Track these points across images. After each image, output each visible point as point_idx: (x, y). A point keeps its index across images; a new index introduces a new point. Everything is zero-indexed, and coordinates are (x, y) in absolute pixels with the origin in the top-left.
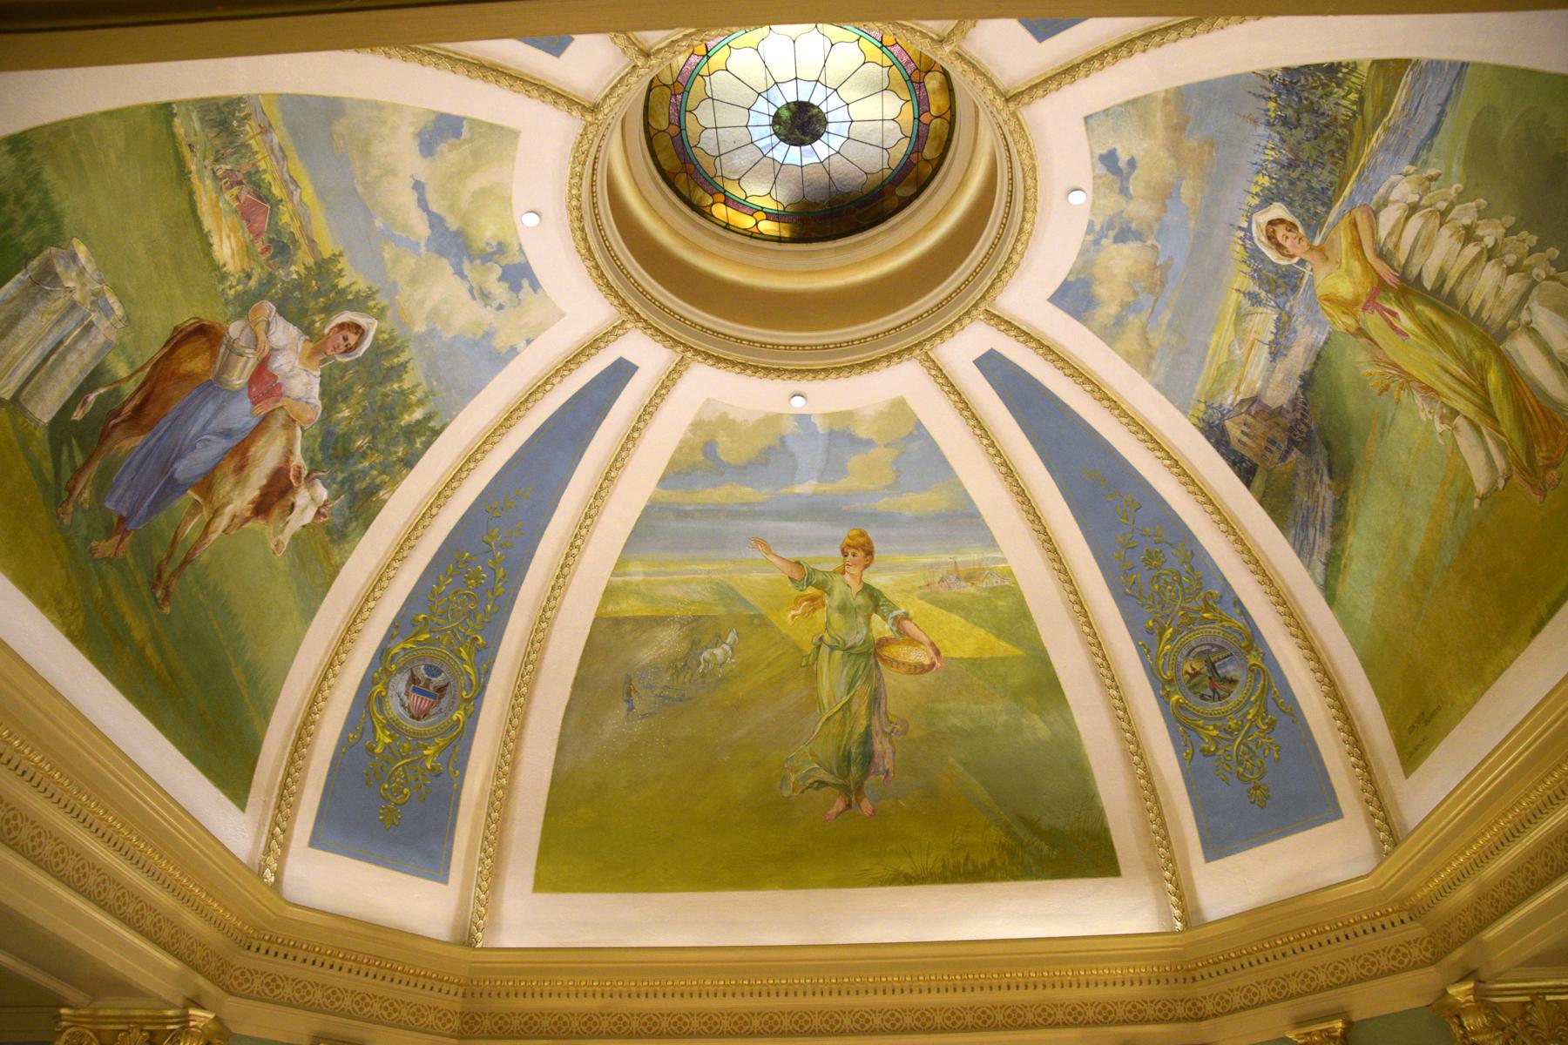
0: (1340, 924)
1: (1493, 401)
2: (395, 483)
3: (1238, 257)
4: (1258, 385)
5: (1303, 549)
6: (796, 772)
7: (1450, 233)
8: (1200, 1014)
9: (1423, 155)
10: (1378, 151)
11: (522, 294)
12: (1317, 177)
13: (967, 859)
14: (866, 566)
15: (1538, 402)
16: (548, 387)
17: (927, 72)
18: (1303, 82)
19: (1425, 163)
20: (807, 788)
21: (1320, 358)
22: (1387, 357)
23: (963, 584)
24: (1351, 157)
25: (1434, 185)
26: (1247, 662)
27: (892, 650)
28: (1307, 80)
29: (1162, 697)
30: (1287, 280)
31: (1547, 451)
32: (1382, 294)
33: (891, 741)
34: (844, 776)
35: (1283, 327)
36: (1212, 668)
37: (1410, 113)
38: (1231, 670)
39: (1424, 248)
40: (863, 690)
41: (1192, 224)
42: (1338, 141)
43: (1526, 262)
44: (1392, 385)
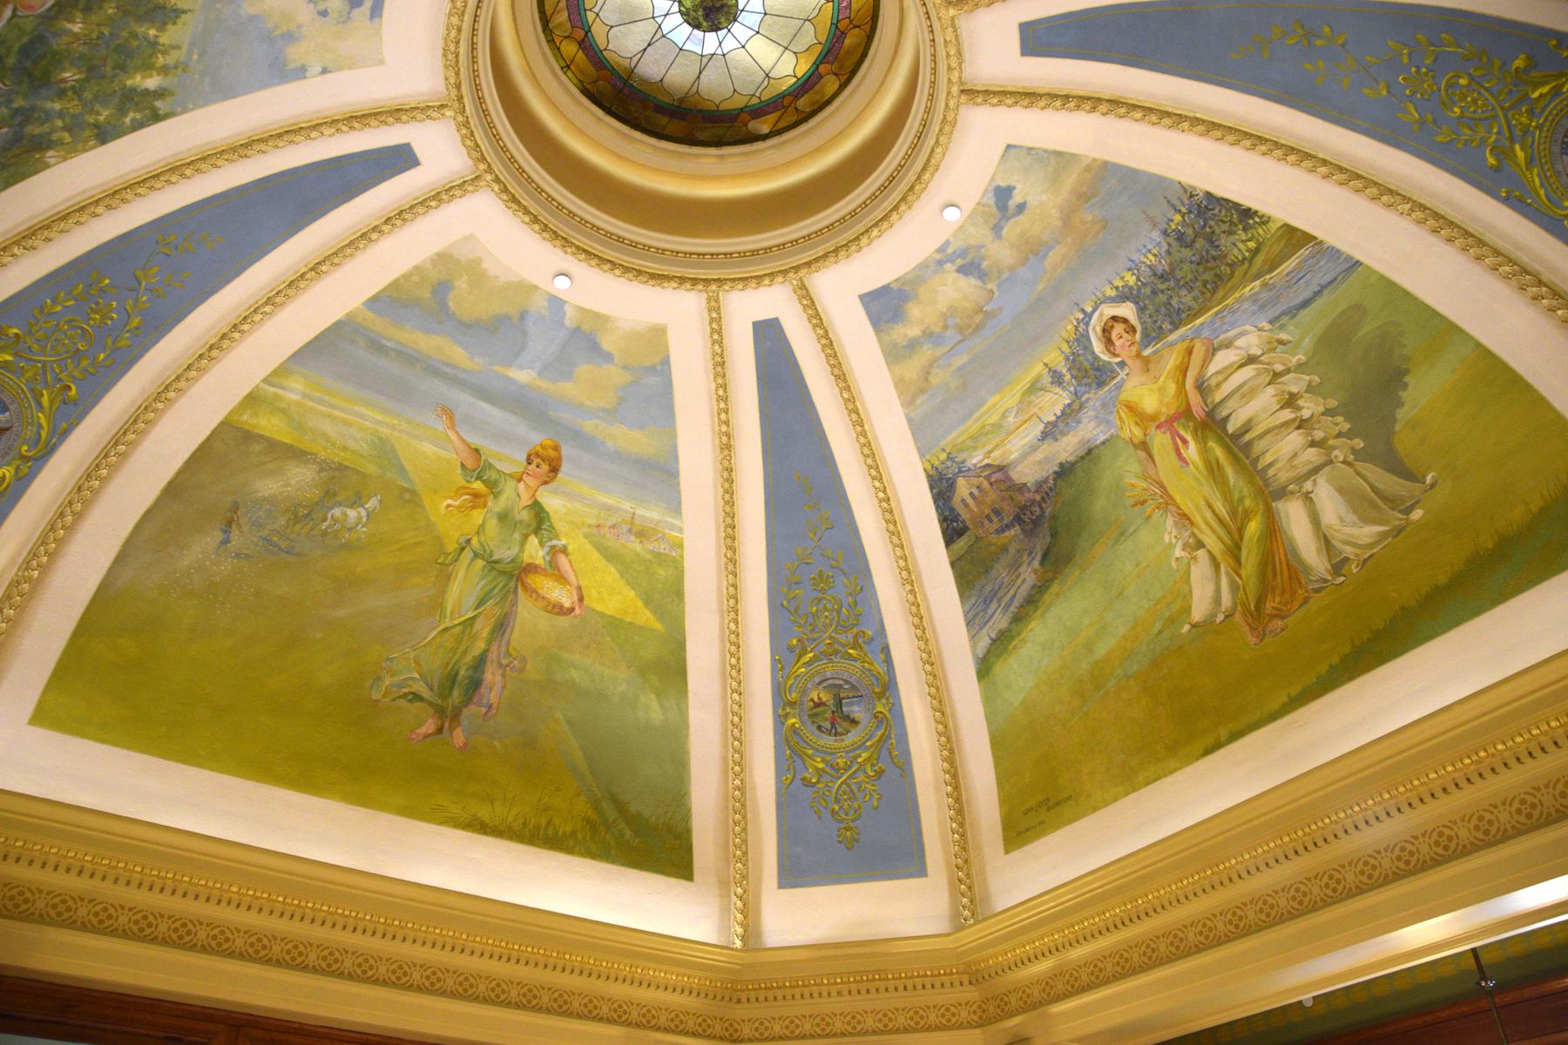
0: (800, 983)
1: (1243, 547)
2: (73, 150)
3: (1065, 335)
4: (1013, 457)
5: (973, 621)
6: (392, 676)
7: (1274, 393)
8: (736, 1036)
9: (1285, 319)
10: (1247, 299)
11: (356, 13)
12: (1180, 297)
13: (549, 823)
14: (545, 483)
15: (1287, 560)
16: (314, 134)
17: (855, 27)
18: (1216, 211)
19: (1282, 327)
20: (400, 697)
21: (1089, 454)
22: (1158, 477)
23: (632, 538)
24: (1220, 294)
25: (1281, 348)
26: (874, 708)
27: (537, 580)
28: (1220, 211)
29: (780, 716)
30: (1098, 373)
31: (1279, 603)
32: (1183, 420)
33: (503, 675)
34: (443, 697)
35: (1069, 415)
36: (839, 702)
37: (1294, 279)
38: (856, 711)
39: (1243, 396)
40: (492, 609)
41: (1040, 287)
42: (1216, 275)
43: (1331, 442)
44: (1150, 502)
